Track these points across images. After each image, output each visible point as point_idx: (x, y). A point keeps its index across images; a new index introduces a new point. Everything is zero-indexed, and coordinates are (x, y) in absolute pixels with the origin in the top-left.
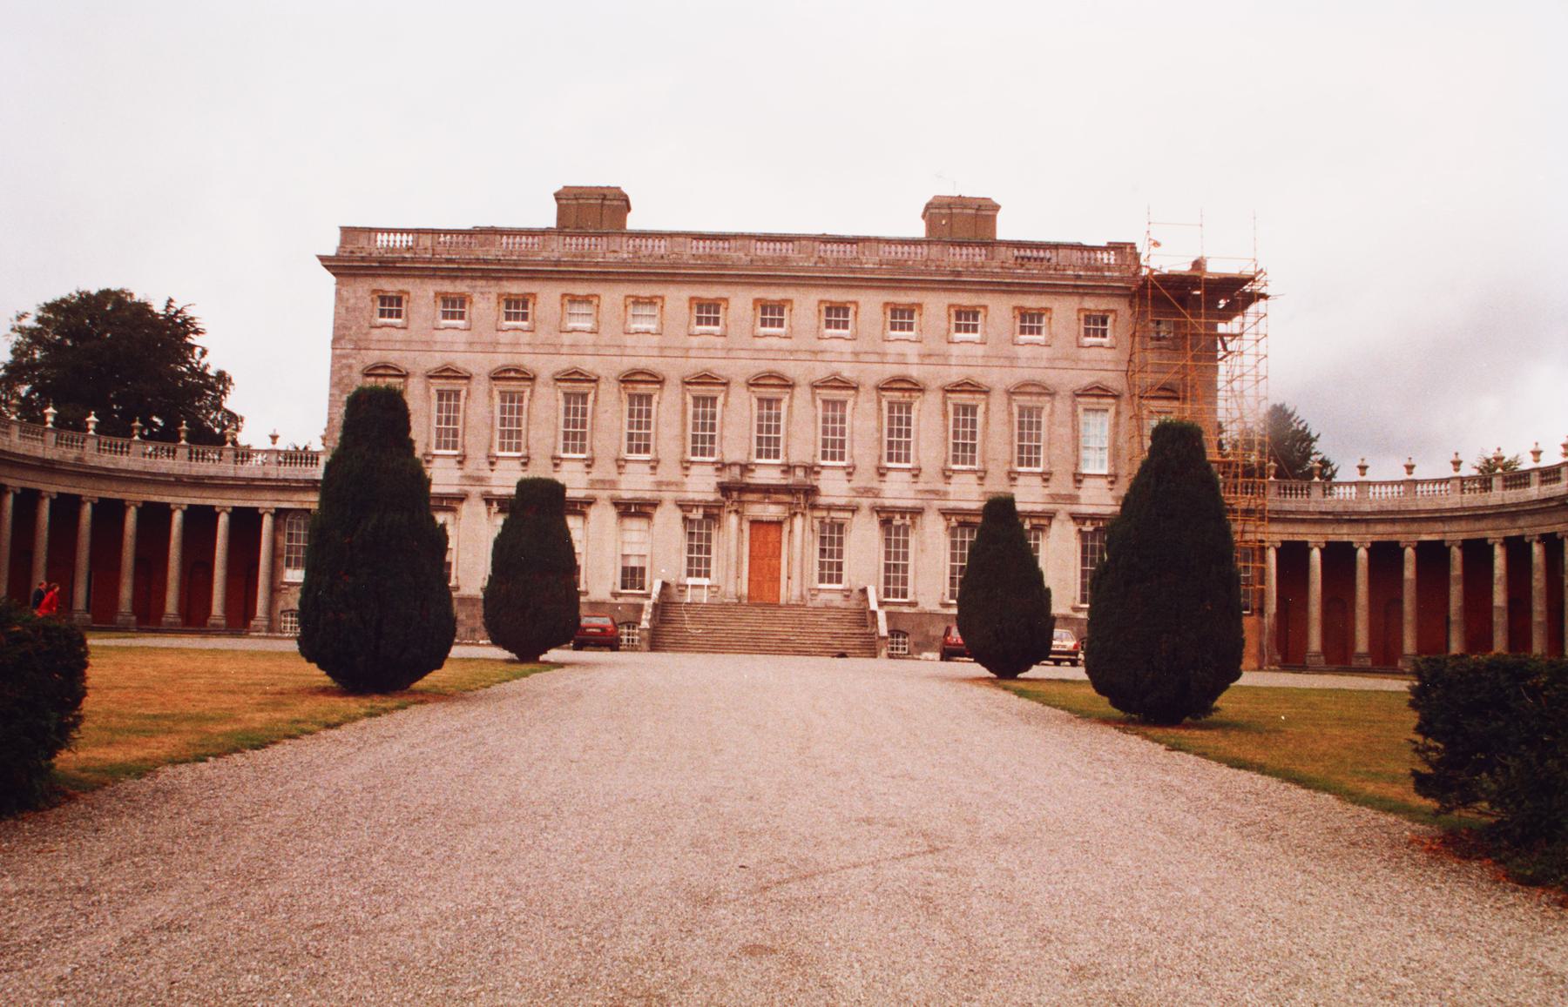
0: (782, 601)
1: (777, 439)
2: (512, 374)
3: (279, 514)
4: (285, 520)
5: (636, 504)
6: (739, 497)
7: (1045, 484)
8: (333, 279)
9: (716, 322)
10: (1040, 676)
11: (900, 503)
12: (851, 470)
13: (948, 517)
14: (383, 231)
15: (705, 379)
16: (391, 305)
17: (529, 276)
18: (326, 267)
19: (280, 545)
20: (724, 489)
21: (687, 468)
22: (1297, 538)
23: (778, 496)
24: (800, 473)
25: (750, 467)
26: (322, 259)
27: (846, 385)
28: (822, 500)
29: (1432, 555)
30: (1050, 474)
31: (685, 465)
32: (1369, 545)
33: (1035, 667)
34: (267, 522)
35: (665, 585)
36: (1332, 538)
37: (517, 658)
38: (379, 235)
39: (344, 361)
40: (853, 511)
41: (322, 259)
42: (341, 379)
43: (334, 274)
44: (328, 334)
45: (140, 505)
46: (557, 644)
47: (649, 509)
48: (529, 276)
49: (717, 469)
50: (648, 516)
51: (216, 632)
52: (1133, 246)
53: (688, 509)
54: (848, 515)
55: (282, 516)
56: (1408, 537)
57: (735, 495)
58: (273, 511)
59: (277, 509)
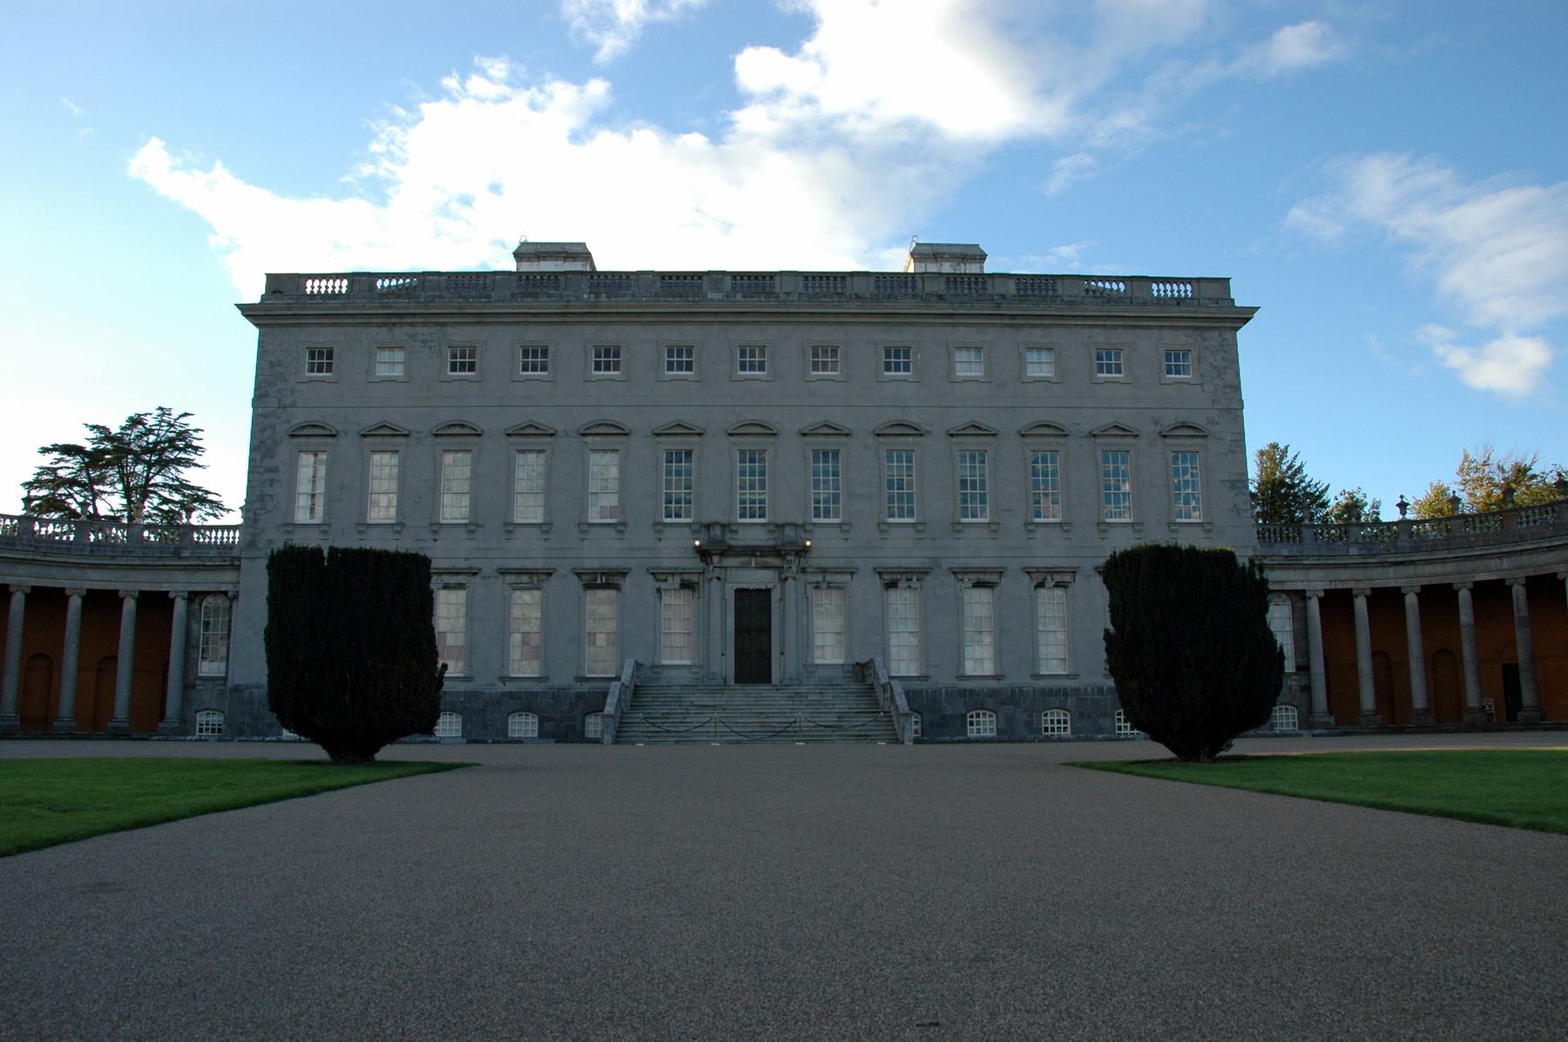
0: (224, 675)
1: (910, 496)
2: (457, 430)
3: (194, 597)
4: (200, 605)
5: (602, 574)
6: (720, 562)
7: (621, 537)
8: (255, 331)
9: (689, 367)
10: (389, 758)
11: (905, 563)
12: (325, 528)
13: (960, 577)
14: (314, 277)
15: (683, 429)
16: (323, 358)
17: (476, 320)
18: (247, 316)
19: (194, 635)
20: (703, 553)
21: (435, 532)
22: (1339, 586)
23: (766, 559)
24: (717, 531)
25: (808, 528)
26: (243, 308)
27: (838, 432)
28: (813, 562)
29: (102, 604)
30: (551, 524)
31: (582, 528)
32: (85, 593)
33: (388, 747)
34: (180, 607)
35: (638, 666)
36: (1378, 584)
37: (1173, 755)
38: (1154, 286)
39: (267, 422)
40: (852, 573)
41: (243, 308)
42: (263, 442)
43: (256, 325)
44: (249, 393)
45: (29, 590)
46: (392, 737)
47: (616, 580)
48: (476, 320)
49: (771, 532)
50: (616, 587)
51: (118, 735)
52: (584, 244)
53: (663, 577)
54: (847, 578)
55: (197, 601)
56: (77, 582)
57: (716, 559)
58: (186, 595)
59: (190, 592)
